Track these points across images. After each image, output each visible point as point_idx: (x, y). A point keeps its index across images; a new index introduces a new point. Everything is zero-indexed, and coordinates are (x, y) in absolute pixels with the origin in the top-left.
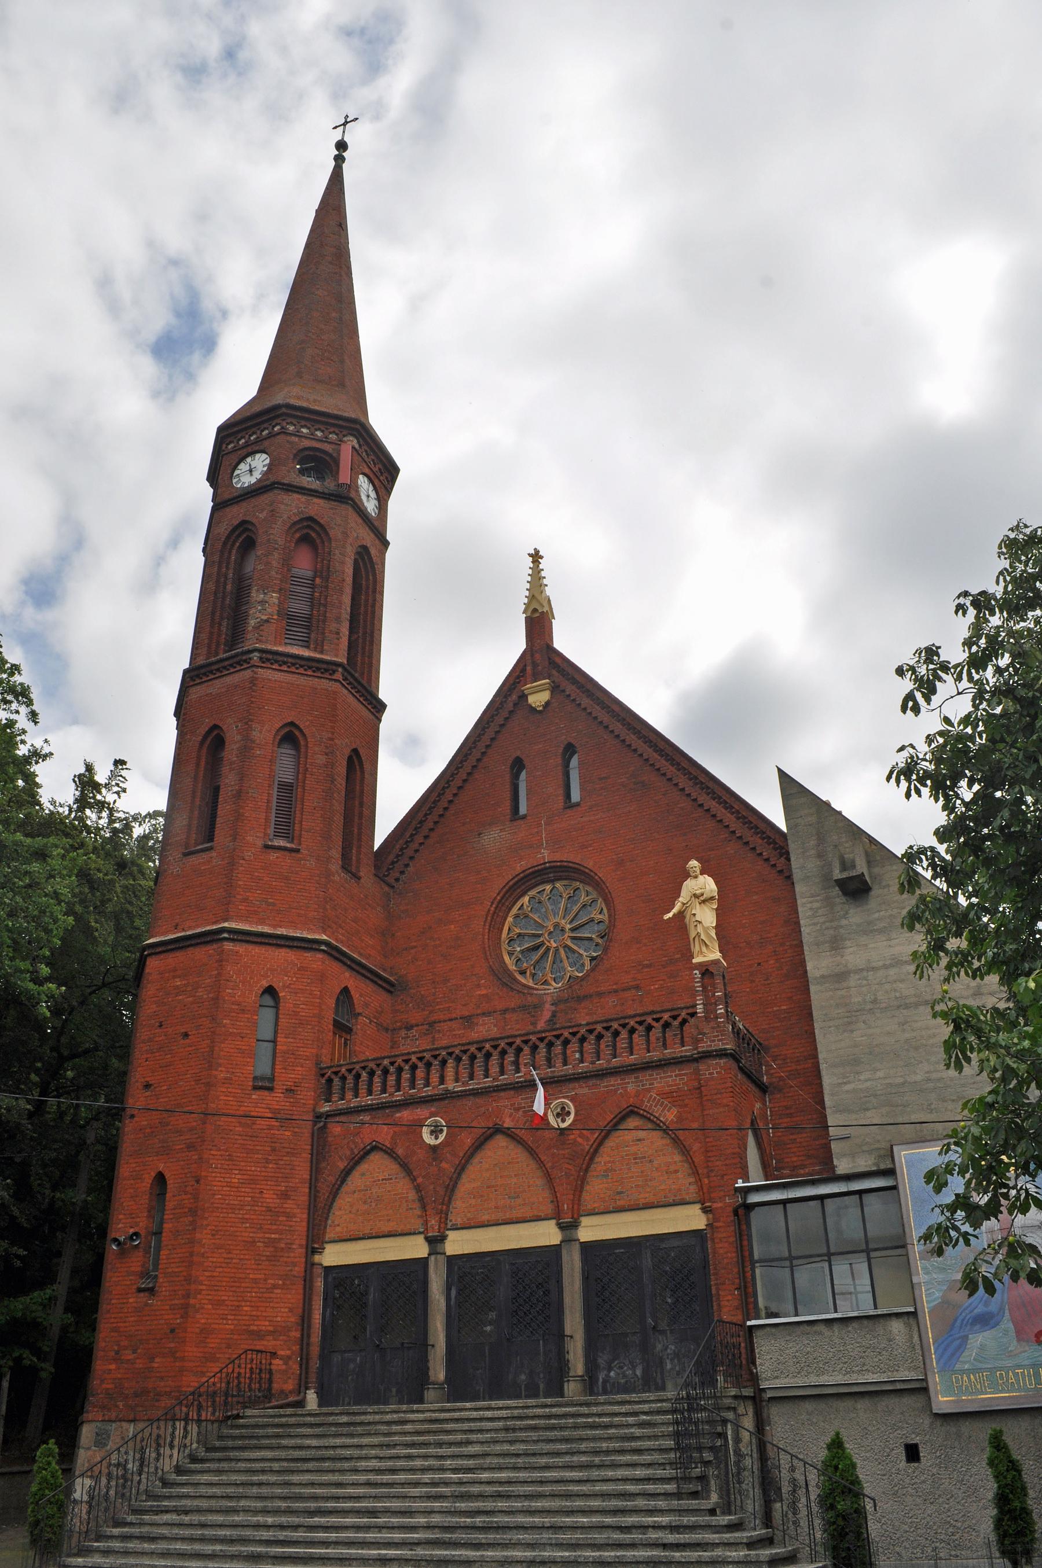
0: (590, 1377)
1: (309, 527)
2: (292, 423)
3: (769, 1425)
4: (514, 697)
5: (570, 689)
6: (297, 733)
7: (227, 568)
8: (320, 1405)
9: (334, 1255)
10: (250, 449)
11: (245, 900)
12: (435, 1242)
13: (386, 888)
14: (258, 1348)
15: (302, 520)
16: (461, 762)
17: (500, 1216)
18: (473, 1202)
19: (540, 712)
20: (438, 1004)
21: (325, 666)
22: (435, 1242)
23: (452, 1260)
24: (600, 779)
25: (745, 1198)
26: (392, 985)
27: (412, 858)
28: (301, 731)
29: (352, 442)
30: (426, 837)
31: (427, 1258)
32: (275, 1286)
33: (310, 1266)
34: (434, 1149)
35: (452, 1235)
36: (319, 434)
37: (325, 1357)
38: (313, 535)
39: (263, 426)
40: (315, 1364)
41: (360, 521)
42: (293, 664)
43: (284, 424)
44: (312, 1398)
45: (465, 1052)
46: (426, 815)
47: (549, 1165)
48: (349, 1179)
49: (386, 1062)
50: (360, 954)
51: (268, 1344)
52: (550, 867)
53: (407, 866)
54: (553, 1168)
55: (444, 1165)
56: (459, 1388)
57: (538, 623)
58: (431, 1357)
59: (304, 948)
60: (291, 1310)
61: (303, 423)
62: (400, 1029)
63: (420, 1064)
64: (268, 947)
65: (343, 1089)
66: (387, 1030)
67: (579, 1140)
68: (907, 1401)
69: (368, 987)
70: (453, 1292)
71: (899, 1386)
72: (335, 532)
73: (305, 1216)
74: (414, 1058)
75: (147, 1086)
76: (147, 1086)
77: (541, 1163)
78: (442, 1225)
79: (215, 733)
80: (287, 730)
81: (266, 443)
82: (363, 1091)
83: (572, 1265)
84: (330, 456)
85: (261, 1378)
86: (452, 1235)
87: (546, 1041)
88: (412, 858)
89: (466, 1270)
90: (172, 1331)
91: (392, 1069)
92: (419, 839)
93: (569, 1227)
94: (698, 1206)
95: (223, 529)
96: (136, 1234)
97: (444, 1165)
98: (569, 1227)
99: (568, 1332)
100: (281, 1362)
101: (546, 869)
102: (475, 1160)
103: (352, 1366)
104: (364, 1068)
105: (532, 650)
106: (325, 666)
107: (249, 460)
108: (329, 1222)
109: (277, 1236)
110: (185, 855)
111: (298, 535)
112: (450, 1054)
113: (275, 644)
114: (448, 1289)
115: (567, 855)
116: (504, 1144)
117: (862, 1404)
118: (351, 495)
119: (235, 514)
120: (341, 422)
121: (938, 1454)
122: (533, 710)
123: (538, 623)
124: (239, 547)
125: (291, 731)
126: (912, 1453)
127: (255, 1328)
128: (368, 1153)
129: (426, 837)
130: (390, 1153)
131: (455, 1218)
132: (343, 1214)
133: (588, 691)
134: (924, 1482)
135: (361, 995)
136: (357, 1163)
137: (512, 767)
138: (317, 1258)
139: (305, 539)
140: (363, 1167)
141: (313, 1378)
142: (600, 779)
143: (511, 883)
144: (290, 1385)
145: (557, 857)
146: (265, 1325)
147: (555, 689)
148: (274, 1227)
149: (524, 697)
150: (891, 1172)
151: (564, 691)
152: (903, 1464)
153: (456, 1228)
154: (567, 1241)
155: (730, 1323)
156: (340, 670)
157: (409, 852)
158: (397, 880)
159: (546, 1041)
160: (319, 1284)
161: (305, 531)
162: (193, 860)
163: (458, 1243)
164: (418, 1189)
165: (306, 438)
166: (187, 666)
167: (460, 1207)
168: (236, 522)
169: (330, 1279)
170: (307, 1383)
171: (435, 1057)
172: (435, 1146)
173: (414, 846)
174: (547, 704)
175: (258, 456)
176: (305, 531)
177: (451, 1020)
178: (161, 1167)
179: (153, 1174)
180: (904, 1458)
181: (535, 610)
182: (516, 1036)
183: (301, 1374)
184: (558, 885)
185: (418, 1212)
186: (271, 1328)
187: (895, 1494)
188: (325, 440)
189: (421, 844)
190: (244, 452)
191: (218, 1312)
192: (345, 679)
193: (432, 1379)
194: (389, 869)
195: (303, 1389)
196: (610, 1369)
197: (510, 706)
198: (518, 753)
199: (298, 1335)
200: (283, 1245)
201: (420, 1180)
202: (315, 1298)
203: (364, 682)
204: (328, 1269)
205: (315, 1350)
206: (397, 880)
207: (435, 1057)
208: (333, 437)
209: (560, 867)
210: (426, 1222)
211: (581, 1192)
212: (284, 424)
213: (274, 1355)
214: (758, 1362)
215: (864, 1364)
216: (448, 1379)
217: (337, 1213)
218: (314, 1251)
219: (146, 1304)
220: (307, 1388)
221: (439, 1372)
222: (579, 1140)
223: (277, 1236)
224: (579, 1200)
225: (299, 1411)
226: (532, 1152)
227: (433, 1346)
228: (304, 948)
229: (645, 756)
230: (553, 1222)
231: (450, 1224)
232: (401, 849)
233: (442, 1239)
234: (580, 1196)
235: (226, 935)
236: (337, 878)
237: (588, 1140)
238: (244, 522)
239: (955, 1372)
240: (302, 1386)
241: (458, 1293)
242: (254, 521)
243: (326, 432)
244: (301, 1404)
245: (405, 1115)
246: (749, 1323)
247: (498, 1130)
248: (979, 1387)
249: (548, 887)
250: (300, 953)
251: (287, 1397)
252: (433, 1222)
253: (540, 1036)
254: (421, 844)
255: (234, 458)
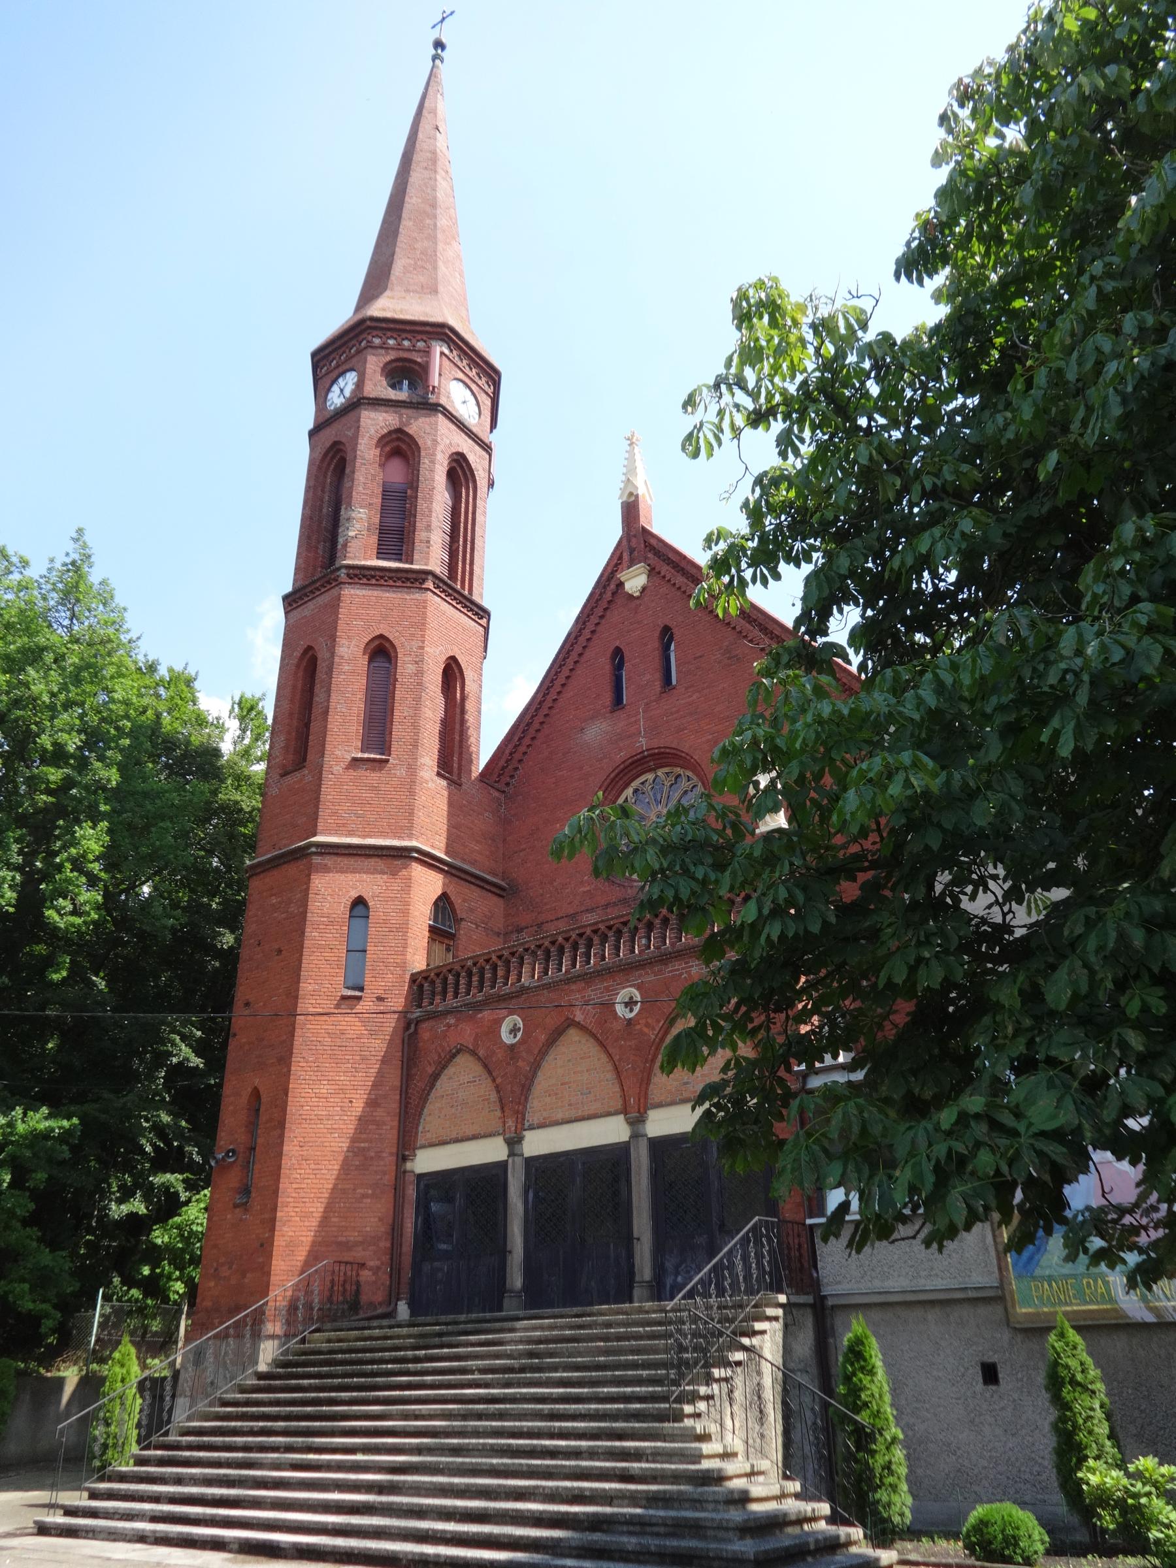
0: (658, 1283)
1: (398, 439)
2: (377, 336)
3: (834, 1336)
4: (613, 586)
5: (665, 569)
6: (387, 645)
7: (323, 491)
8: (412, 1314)
9: (428, 1161)
10: (341, 370)
11: (335, 813)
12: (514, 1143)
13: (496, 794)
14: (345, 1259)
15: (390, 433)
16: (564, 660)
17: (573, 1114)
18: (548, 1099)
19: (638, 598)
20: (546, 904)
21: (414, 576)
22: (514, 1143)
23: (530, 1161)
24: (695, 658)
25: (804, 1083)
26: (503, 889)
27: (520, 761)
28: (391, 642)
29: (438, 348)
30: (533, 739)
31: (507, 1161)
32: (364, 1196)
33: (401, 1174)
34: (512, 1047)
35: (529, 1135)
36: (406, 343)
37: (416, 1267)
38: (404, 447)
39: (350, 344)
40: (407, 1274)
41: (453, 427)
42: (382, 577)
43: (370, 338)
44: (403, 1310)
45: (539, 947)
46: (533, 716)
47: (616, 1058)
48: (438, 1084)
49: (470, 963)
50: (463, 860)
51: (359, 1254)
52: (649, 755)
53: (516, 769)
54: (620, 1060)
55: (520, 1063)
56: (537, 1298)
57: (631, 510)
58: (509, 1263)
59: (394, 856)
60: (380, 1220)
61: (389, 334)
62: (512, 932)
63: (499, 963)
64: (357, 858)
65: (433, 994)
66: (498, 934)
67: (646, 1030)
68: (983, 1311)
69: (474, 893)
70: (531, 1195)
71: (971, 1294)
72: (424, 441)
73: (396, 1123)
74: (494, 958)
75: (247, 1004)
76: (247, 1004)
77: (610, 1056)
78: (519, 1126)
79: (310, 653)
80: (377, 643)
81: (354, 360)
82: (450, 995)
83: (641, 1160)
84: (419, 364)
85: (345, 1290)
86: (529, 1135)
87: (614, 929)
88: (520, 761)
89: (548, 1172)
90: (262, 1245)
91: (475, 970)
92: (527, 741)
93: (636, 1121)
94: (621, 1117)
95: (320, 451)
96: (233, 1151)
97: (520, 1063)
98: (636, 1121)
99: (635, 1235)
100: (370, 1273)
101: (645, 757)
102: (550, 1058)
103: (440, 1275)
104: (450, 971)
105: (628, 534)
106: (414, 576)
107: (340, 380)
108: (420, 1129)
109: (366, 1145)
110: (282, 776)
111: (388, 449)
112: (526, 950)
113: (365, 559)
114: (526, 1192)
115: (667, 740)
116: (577, 1038)
117: (932, 1315)
118: (441, 402)
119: (329, 436)
120: (428, 328)
121: (1020, 1375)
122: (631, 596)
123: (631, 510)
124: (334, 469)
125: (381, 644)
126: (990, 1374)
127: (344, 1239)
128: (454, 1056)
129: (533, 739)
130: (474, 1053)
131: (532, 1117)
132: (432, 1120)
133: (683, 569)
134: (1003, 1409)
135: (464, 901)
136: (444, 1067)
137: (613, 658)
138: (409, 1165)
139: (397, 453)
140: (450, 1070)
141: (405, 1288)
142: (695, 658)
143: (612, 776)
144: (379, 1297)
145: (655, 743)
146: (353, 1236)
147: (652, 572)
148: (364, 1136)
149: (621, 585)
150: (361, 989)
151: (659, 573)
152: (979, 1386)
153: (531, 1128)
154: (635, 1136)
155: (792, 1223)
156: (430, 577)
157: (517, 756)
158: (508, 784)
159: (614, 929)
160: (411, 1193)
161: (395, 444)
162: (290, 779)
163: (537, 1143)
164: (498, 1089)
165: (393, 349)
166: (289, 588)
167: (537, 1105)
168: (328, 445)
169: (422, 1186)
170: (398, 1294)
171: (513, 954)
172: (512, 1045)
173: (522, 749)
174: (644, 589)
175: (348, 375)
176: (395, 444)
177: (557, 919)
178: (257, 1082)
179: (250, 1090)
180: (980, 1379)
181: (631, 494)
182: (586, 926)
183: (391, 1286)
184: (660, 773)
185: (498, 1113)
186: (360, 1239)
187: (972, 1422)
188: (413, 349)
189: (528, 746)
190: (337, 372)
191: (307, 1224)
192: (438, 587)
193: (508, 1286)
194: (499, 775)
195: (393, 1300)
196: (677, 1274)
197: (608, 596)
198: (617, 643)
199: (388, 1245)
200: (373, 1154)
201: (499, 1080)
202: (406, 1206)
203: (466, 593)
204: (420, 1177)
205: (407, 1260)
206: (508, 784)
207: (513, 954)
208: (421, 345)
209: (659, 754)
210: (504, 1123)
211: (648, 1084)
212: (370, 338)
213: (362, 1265)
214: (820, 1265)
215: (932, 1269)
216: (526, 1287)
217: (428, 1119)
218: (405, 1159)
219: (241, 1220)
220: (398, 1300)
221: (516, 1279)
222: (646, 1030)
223: (366, 1145)
224: (646, 1094)
225: (393, 1322)
226: (602, 1045)
227: (638, 1239)
228: (394, 856)
229: (738, 629)
230: (621, 1117)
231: (527, 1124)
232: (511, 754)
233: (520, 1140)
234: (647, 1089)
235: (313, 849)
236: (431, 785)
237: (653, 1029)
238: (336, 443)
239: (1034, 1278)
240: (392, 1297)
241: (536, 1195)
242: (343, 440)
243: (414, 341)
244: (391, 1315)
245: (486, 1015)
246: (809, 1221)
247: (572, 1023)
248: (1062, 1297)
249: (650, 776)
250: (390, 861)
251: (375, 1308)
252: (510, 1123)
253: (607, 924)
254: (528, 746)
255: (327, 380)
